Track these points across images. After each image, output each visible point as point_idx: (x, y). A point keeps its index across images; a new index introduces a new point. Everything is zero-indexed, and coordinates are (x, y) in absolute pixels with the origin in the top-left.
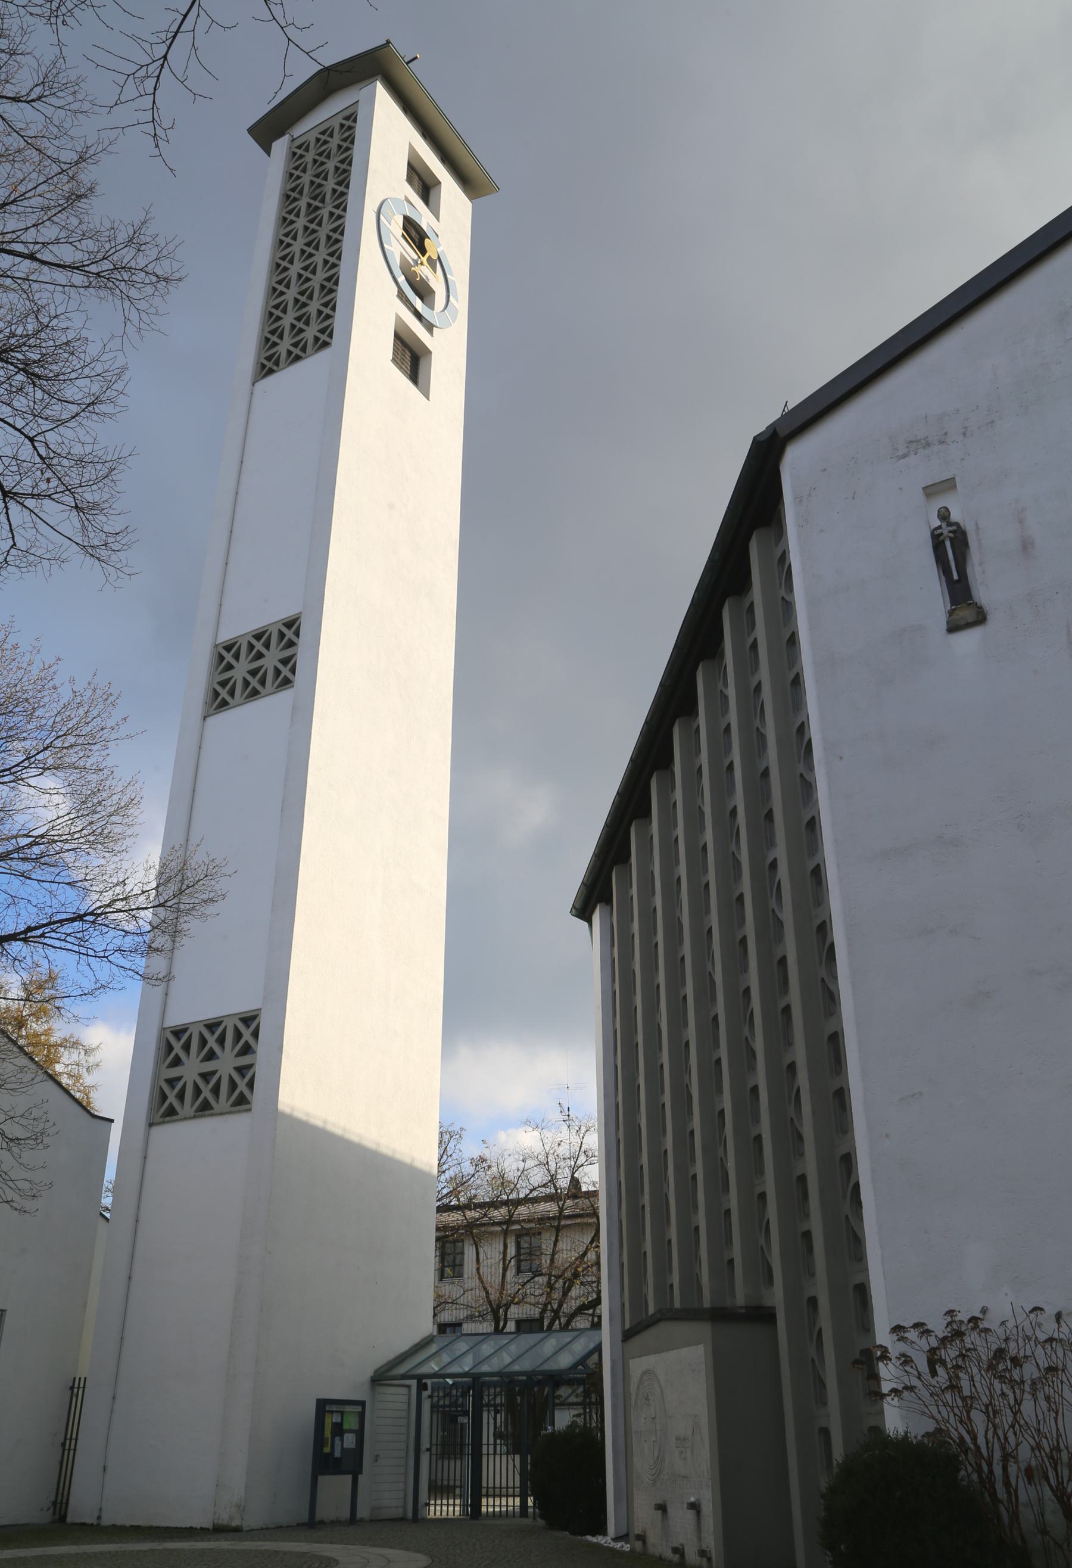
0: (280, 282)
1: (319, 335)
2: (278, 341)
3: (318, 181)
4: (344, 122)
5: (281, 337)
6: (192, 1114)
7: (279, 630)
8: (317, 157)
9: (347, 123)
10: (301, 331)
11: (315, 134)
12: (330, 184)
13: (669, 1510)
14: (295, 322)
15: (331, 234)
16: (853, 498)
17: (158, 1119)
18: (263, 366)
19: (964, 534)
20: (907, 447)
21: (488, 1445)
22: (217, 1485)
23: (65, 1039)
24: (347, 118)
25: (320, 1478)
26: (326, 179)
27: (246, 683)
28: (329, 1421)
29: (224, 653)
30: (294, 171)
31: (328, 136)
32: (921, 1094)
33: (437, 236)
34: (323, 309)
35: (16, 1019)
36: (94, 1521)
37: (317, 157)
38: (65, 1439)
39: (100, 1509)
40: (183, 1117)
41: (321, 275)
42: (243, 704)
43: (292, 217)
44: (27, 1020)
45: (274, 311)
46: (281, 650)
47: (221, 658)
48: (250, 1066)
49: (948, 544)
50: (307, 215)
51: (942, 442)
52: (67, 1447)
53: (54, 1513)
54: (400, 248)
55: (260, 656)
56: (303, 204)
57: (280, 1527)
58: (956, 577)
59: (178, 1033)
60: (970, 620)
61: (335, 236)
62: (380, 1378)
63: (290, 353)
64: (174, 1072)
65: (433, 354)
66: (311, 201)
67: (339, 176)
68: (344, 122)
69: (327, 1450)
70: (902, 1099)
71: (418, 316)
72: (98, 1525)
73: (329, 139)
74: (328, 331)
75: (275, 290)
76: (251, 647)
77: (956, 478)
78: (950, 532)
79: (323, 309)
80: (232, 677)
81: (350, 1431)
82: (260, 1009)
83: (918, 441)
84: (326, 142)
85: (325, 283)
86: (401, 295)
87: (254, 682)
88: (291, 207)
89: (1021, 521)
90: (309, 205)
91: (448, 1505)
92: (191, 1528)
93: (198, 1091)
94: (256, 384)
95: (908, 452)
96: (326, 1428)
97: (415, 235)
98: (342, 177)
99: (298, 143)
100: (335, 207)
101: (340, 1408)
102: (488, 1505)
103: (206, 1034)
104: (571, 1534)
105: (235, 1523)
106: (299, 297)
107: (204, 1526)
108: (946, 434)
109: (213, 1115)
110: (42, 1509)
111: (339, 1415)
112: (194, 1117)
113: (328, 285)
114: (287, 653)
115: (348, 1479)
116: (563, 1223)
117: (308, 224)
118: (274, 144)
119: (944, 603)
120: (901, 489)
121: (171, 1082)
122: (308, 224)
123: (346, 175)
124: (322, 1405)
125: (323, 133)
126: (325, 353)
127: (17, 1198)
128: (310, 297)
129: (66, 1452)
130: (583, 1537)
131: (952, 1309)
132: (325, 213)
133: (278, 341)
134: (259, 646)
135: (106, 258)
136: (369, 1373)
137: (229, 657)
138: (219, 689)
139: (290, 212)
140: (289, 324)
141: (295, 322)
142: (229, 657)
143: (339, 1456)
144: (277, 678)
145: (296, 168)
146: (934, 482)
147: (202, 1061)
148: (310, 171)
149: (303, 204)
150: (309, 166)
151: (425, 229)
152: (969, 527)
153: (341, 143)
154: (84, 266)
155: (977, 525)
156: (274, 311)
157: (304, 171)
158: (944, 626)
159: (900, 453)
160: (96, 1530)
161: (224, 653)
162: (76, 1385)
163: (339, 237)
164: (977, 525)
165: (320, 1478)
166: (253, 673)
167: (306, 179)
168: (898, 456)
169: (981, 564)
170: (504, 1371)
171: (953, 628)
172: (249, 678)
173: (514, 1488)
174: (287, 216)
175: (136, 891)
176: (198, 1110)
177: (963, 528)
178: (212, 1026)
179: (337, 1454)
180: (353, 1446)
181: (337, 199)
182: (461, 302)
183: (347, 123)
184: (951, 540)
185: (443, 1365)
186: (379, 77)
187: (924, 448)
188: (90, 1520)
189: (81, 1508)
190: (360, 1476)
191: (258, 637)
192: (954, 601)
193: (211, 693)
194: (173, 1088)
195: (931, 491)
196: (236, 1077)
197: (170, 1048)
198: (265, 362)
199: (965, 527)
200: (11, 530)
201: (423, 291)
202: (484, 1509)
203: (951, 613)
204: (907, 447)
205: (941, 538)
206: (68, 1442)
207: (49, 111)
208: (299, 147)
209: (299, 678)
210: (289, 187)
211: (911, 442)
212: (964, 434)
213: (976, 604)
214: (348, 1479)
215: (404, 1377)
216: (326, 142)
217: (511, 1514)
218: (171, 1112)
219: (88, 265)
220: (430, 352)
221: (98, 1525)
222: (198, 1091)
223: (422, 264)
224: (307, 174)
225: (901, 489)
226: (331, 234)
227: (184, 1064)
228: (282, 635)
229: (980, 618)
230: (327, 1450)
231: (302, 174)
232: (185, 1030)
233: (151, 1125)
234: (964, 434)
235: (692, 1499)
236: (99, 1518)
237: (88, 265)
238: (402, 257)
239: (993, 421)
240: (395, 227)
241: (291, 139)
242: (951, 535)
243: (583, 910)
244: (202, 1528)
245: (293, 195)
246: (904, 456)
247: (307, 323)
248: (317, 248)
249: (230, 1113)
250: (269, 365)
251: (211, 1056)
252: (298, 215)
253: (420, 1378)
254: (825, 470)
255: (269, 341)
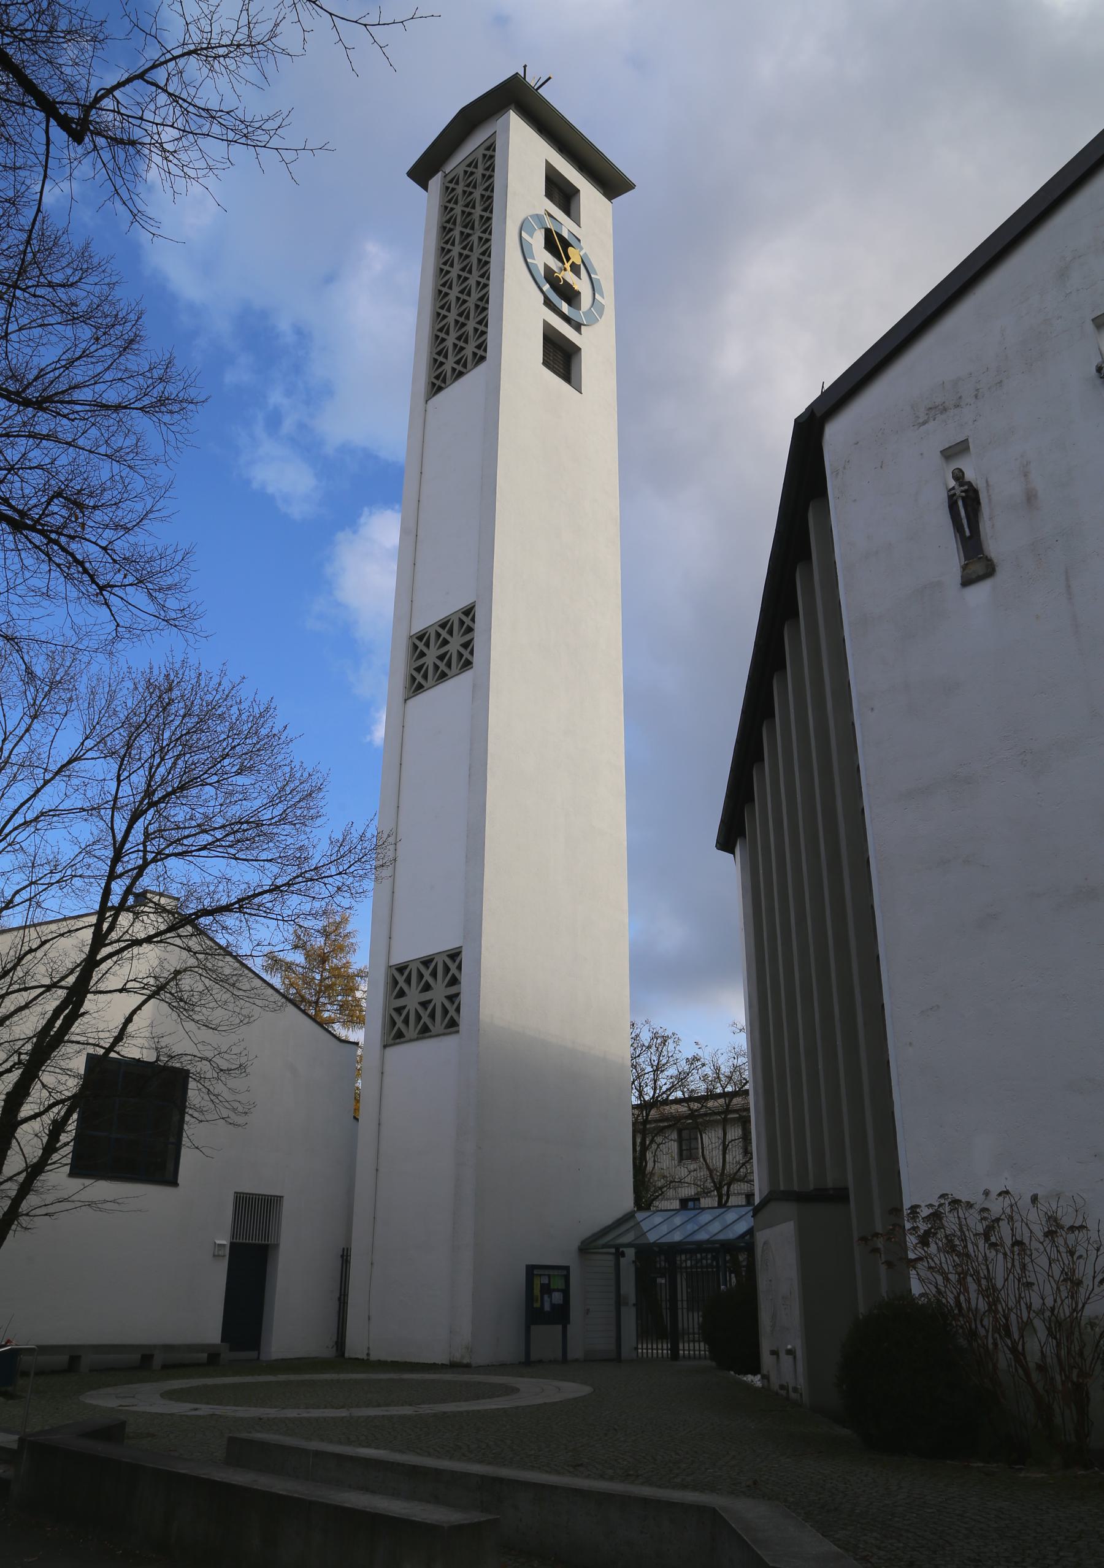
0: (442, 307)
1: (476, 350)
2: (444, 360)
3: (468, 210)
4: (486, 152)
5: (446, 357)
6: (416, 1036)
7: (436, 631)
8: (466, 189)
9: (488, 153)
10: (462, 349)
11: (463, 167)
12: (478, 212)
13: (780, 1354)
14: (457, 342)
15: (481, 257)
16: (881, 467)
17: (391, 1042)
18: (434, 384)
19: (976, 492)
20: (927, 414)
21: (682, 1300)
22: (451, 1332)
23: (360, 970)
24: (488, 149)
25: (533, 1327)
26: (474, 207)
27: (436, 667)
28: (537, 1284)
29: (417, 642)
30: (448, 204)
31: (474, 167)
32: (938, 1006)
33: (579, 240)
34: (478, 326)
35: (319, 956)
36: (365, 1357)
37: (466, 189)
38: (341, 1295)
39: (369, 1348)
40: (409, 1039)
41: (475, 295)
42: (433, 686)
43: (448, 247)
44: (328, 956)
45: (439, 334)
46: (462, 636)
47: (416, 647)
48: (458, 995)
49: (960, 503)
50: (461, 242)
51: (957, 406)
52: (342, 1301)
53: (337, 1350)
54: (543, 258)
55: (445, 642)
56: (456, 233)
57: (505, 1364)
58: (968, 533)
59: (401, 969)
60: (981, 573)
61: (484, 258)
62: (587, 1248)
63: (454, 370)
64: (400, 1003)
65: (582, 350)
66: (464, 230)
67: (484, 203)
68: (486, 152)
69: (537, 1305)
70: (922, 1011)
71: (567, 319)
72: (368, 1360)
73: (474, 170)
74: (482, 346)
75: (438, 314)
76: (438, 635)
77: (969, 440)
78: (962, 492)
79: (478, 326)
80: (425, 663)
81: (558, 1290)
82: (461, 947)
83: (936, 407)
84: (472, 173)
85: (479, 303)
86: (548, 303)
87: (442, 666)
88: (447, 238)
89: (1026, 475)
90: (462, 233)
91: (657, 1349)
92: (434, 1364)
93: (419, 1017)
94: (429, 402)
95: (928, 418)
96: (535, 1286)
97: (556, 244)
98: (487, 203)
99: (449, 178)
100: (482, 232)
101: (546, 1272)
102: (684, 1349)
103: (422, 969)
104: (735, 1373)
105: (465, 1361)
106: (458, 318)
107: (444, 1362)
108: (960, 397)
109: (431, 1037)
110: (327, 1347)
111: (547, 1277)
112: (417, 1039)
113: (481, 304)
114: (467, 638)
115: (559, 1327)
116: (730, 1116)
117: (462, 251)
118: (429, 182)
119: (959, 559)
120: (922, 454)
121: (399, 1010)
122: (462, 251)
123: (489, 201)
124: (532, 1271)
125: (469, 165)
126: (483, 366)
127: (232, 1114)
128: (467, 318)
129: (342, 1305)
130: (740, 1376)
131: (945, 1192)
132: (475, 239)
133: (444, 360)
134: (444, 634)
135: (147, 394)
136: (576, 1244)
137: (421, 646)
138: (415, 674)
139: (447, 242)
140: (452, 344)
141: (457, 342)
142: (421, 646)
143: (549, 1309)
144: (461, 660)
145: (449, 201)
146: (951, 445)
147: (421, 992)
148: (461, 203)
149: (456, 233)
150: (460, 198)
151: (567, 238)
152: (980, 485)
153: (485, 172)
154: (130, 404)
155: (987, 482)
156: (439, 334)
157: (456, 203)
158: (958, 580)
159: (921, 420)
160: (365, 1364)
161: (417, 642)
162: (345, 1254)
163: (488, 259)
164: (987, 482)
165: (533, 1327)
166: (441, 658)
167: (458, 209)
168: (918, 424)
169: (991, 519)
170: (659, 1241)
171: (967, 582)
172: (438, 663)
173: (694, 1334)
174: (444, 246)
175: (325, 861)
176: (420, 1033)
177: (975, 487)
178: (427, 962)
179: (547, 1307)
180: (561, 1302)
181: (484, 224)
182: (608, 299)
183: (488, 153)
184: (963, 499)
185: (687, 1234)
186: (513, 106)
187: (941, 413)
188: (362, 1355)
189: (355, 1346)
190: (568, 1326)
191: (443, 625)
192: (967, 557)
193: (409, 678)
194: (400, 1014)
195: (951, 453)
196: (447, 1004)
197: (395, 982)
198: (435, 381)
199: (977, 485)
200: (113, 615)
201: (570, 295)
202: (681, 1352)
203: (964, 568)
204: (927, 414)
205: (955, 498)
206: (342, 1297)
207: (88, 288)
208: (451, 182)
209: (477, 659)
210: (445, 219)
211: (931, 408)
212: (976, 396)
213: (987, 557)
214: (559, 1327)
215: (605, 1246)
216: (472, 173)
217: (697, 1356)
218: (400, 1035)
219: (134, 403)
220: (580, 349)
221: (368, 1360)
222: (419, 1017)
223: (565, 270)
224: (459, 204)
225: (922, 454)
226: (481, 257)
227: (432, 989)
228: (462, 623)
229: (989, 570)
230: (537, 1305)
231: (454, 206)
232: (406, 967)
233: (385, 1047)
234: (976, 396)
235: (789, 1347)
236: (368, 1355)
237: (134, 403)
238: (547, 267)
239: (1001, 381)
240: (537, 241)
241: (444, 175)
242: (963, 494)
243: (726, 842)
244: (442, 1364)
245: (449, 226)
246: (924, 423)
247: (466, 341)
248: (470, 272)
249: (444, 1034)
250: (438, 383)
251: (427, 987)
252: (453, 244)
253: (617, 1247)
254: (858, 443)
255: (436, 363)
